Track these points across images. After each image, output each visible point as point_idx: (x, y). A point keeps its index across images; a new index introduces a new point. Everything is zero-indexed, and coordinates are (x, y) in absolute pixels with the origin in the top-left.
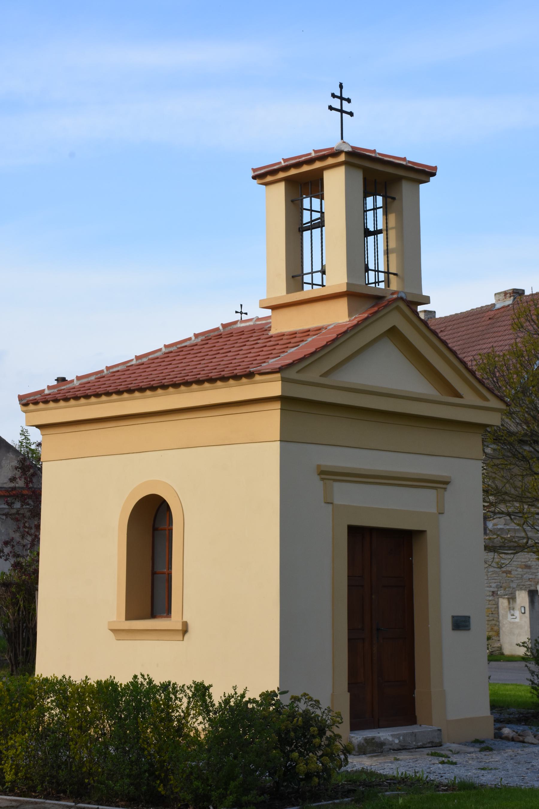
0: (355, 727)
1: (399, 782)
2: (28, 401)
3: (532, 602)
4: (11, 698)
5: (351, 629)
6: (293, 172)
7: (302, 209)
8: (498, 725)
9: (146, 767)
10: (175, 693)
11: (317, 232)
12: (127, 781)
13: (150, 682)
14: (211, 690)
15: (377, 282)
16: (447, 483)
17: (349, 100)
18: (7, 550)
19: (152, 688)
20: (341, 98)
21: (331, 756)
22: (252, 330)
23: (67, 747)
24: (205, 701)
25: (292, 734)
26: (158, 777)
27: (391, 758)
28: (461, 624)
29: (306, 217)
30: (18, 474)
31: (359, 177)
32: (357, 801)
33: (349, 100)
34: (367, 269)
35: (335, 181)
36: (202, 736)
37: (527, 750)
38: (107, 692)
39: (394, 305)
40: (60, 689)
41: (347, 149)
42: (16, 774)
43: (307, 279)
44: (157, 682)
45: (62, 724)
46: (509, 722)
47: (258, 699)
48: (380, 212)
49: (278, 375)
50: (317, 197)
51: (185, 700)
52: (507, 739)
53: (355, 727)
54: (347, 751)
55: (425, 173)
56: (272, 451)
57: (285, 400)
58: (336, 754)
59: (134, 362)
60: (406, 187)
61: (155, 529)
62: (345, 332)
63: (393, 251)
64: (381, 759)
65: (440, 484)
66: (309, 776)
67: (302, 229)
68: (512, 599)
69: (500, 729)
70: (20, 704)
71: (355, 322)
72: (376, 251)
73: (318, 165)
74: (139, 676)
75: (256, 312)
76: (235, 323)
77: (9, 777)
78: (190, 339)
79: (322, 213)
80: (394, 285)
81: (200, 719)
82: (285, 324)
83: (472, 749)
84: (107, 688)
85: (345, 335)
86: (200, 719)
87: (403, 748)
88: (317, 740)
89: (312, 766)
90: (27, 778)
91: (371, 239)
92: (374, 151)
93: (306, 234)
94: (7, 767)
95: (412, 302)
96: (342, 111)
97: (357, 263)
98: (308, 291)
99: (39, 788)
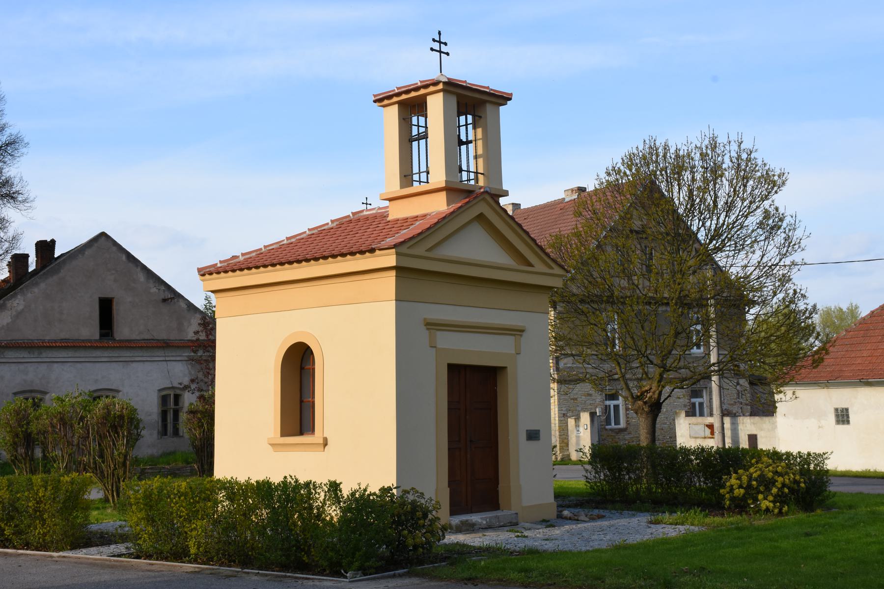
0: (453, 513)
1: (484, 551)
2: (205, 272)
3: (592, 421)
4: (193, 493)
5: (450, 442)
6: (404, 97)
7: (412, 125)
8: (560, 509)
9: (293, 543)
10: (315, 488)
11: (422, 142)
12: (279, 553)
13: (297, 481)
14: (341, 486)
15: (469, 180)
16: (523, 331)
17: (446, 44)
18: (193, 386)
19: (297, 486)
20: (440, 42)
21: (432, 532)
22: (375, 217)
23: (235, 528)
24: (336, 495)
25: (403, 517)
26: (303, 550)
27: (480, 535)
28: (533, 435)
29: (415, 131)
30: (200, 329)
31: (454, 101)
32: (452, 564)
33: (446, 44)
34: (461, 170)
35: (436, 104)
36: (335, 520)
37: (579, 526)
38: (264, 489)
39: (481, 197)
40: (233, 489)
41: (446, 80)
42: (198, 549)
43: (416, 177)
44: (302, 481)
45: (231, 513)
46: (568, 507)
47: (378, 492)
48: (470, 127)
49: (394, 250)
50: (422, 116)
51: (322, 494)
52: (566, 518)
53: (453, 513)
54: (444, 529)
55: (503, 99)
56: (391, 307)
57: (399, 269)
58: (436, 531)
59: (285, 242)
60: (489, 108)
61: (302, 368)
62: (444, 218)
63: (481, 156)
64: (473, 535)
65: (517, 332)
66: (416, 547)
67: (411, 140)
68: (577, 419)
69: (561, 511)
70: (200, 498)
71: (452, 210)
72: (469, 158)
73: (422, 92)
74: (288, 477)
75: (378, 204)
76: (362, 211)
77: (193, 551)
78: (327, 224)
79: (426, 127)
80: (481, 183)
81: (334, 507)
82: (398, 211)
83: (539, 526)
84: (264, 485)
85: (444, 220)
86: (334, 507)
87: (489, 527)
88: (422, 522)
89: (418, 540)
90: (206, 552)
91: (464, 148)
92: (465, 82)
93: (415, 144)
94: (191, 543)
95: (495, 194)
96: (440, 52)
97: (453, 166)
98: (416, 187)
99: (215, 558)
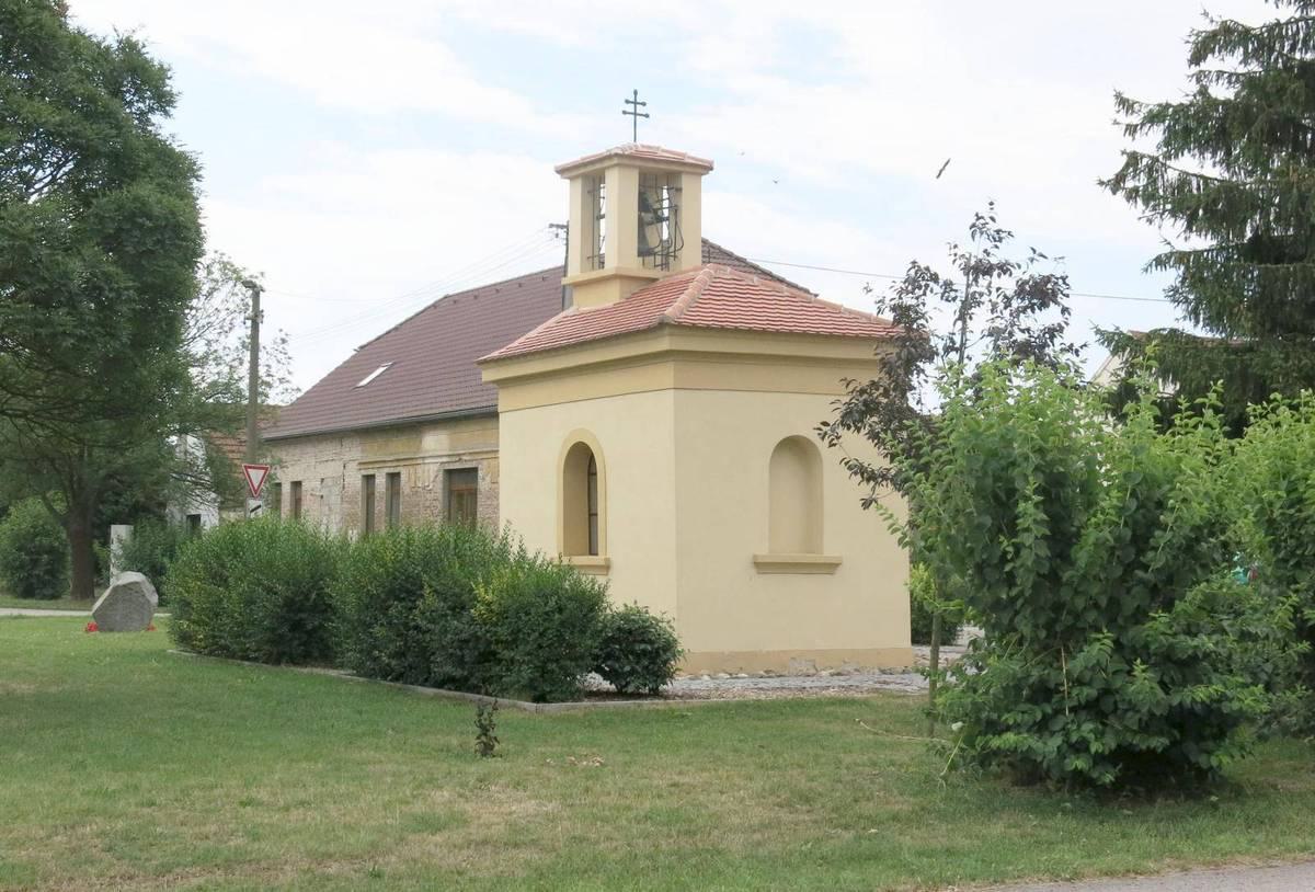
6: (590, 168)
16: (837, 565)
17: (644, 104)
73: (598, 166)
